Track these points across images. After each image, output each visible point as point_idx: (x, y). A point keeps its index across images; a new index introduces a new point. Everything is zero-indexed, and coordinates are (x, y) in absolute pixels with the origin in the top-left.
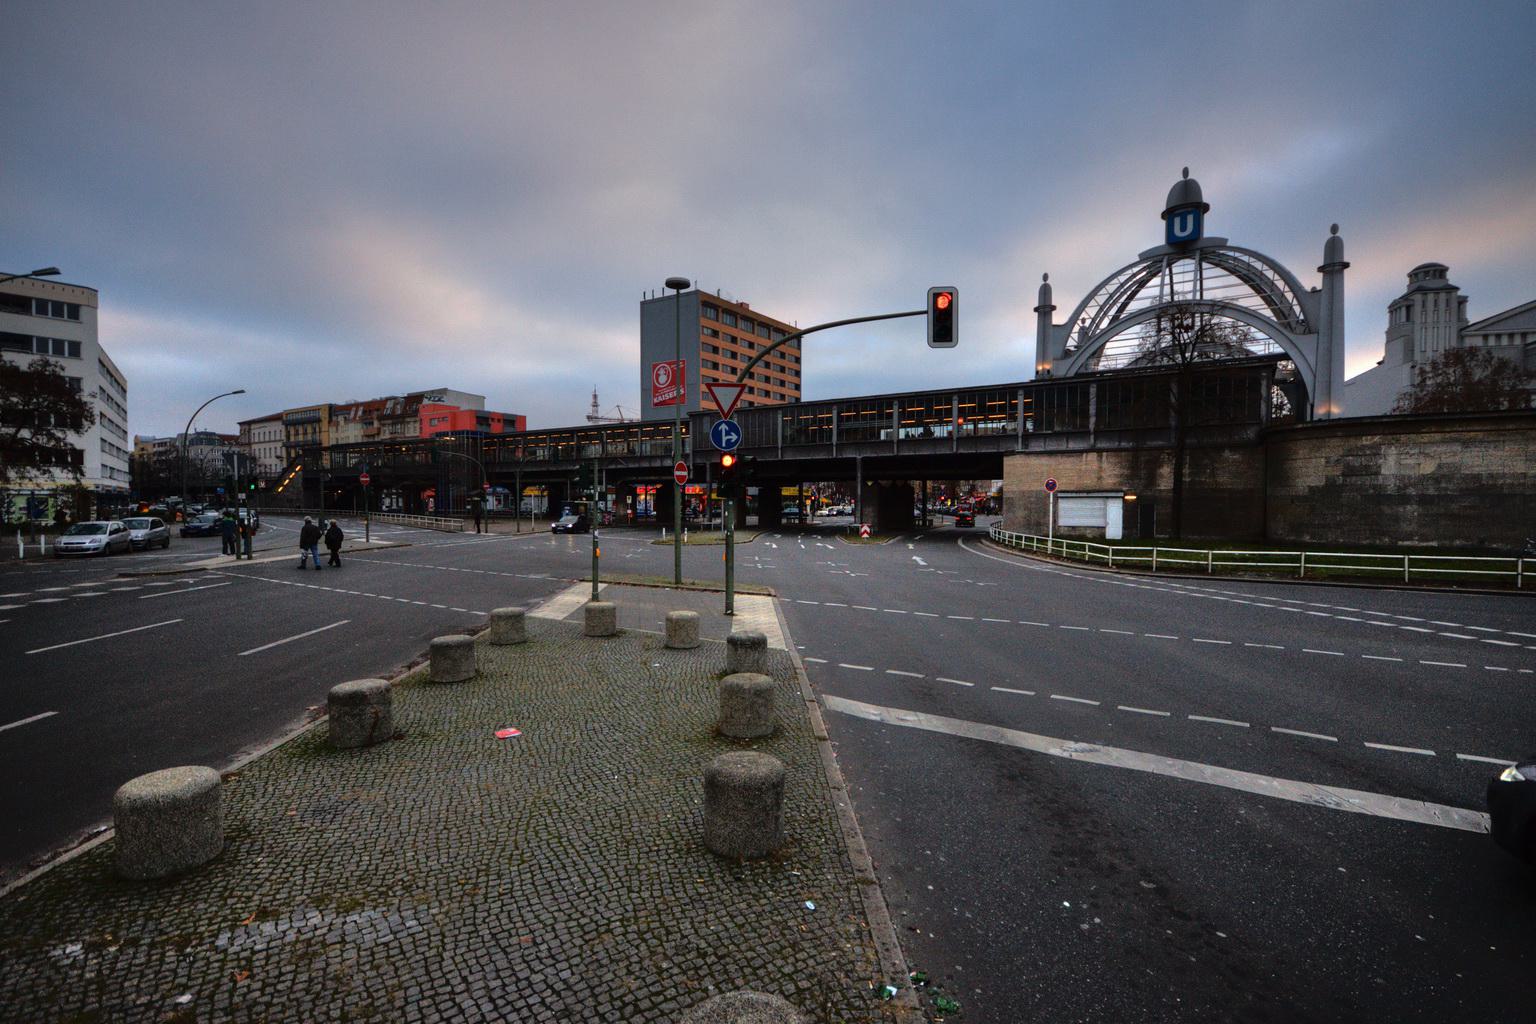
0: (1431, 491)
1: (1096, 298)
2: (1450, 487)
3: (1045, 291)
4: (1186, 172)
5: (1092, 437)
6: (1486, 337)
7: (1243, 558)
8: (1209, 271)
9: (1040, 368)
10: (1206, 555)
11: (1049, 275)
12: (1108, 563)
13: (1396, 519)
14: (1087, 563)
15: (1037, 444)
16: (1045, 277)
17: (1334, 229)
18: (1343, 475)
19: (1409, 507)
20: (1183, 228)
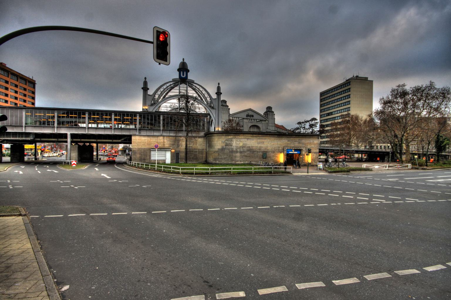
0: (242, 150)
1: (161, 89)
2: (245, 149)
3: (145, 83)
4: (183, 59)
5: (161, 131)
6: (233, 117)
7: (220, 169)
8: (189, 89)
9: (144, 108)
10: (194, 168)
11: (147, 78)
12: (180, 173)
13: (235, 157)
14: (172, 173)
15: (144, 133)
16: (145, 78)
17: (219, 84)
18: (225, 146)
19: (238, 154)
20: (183, 75)
